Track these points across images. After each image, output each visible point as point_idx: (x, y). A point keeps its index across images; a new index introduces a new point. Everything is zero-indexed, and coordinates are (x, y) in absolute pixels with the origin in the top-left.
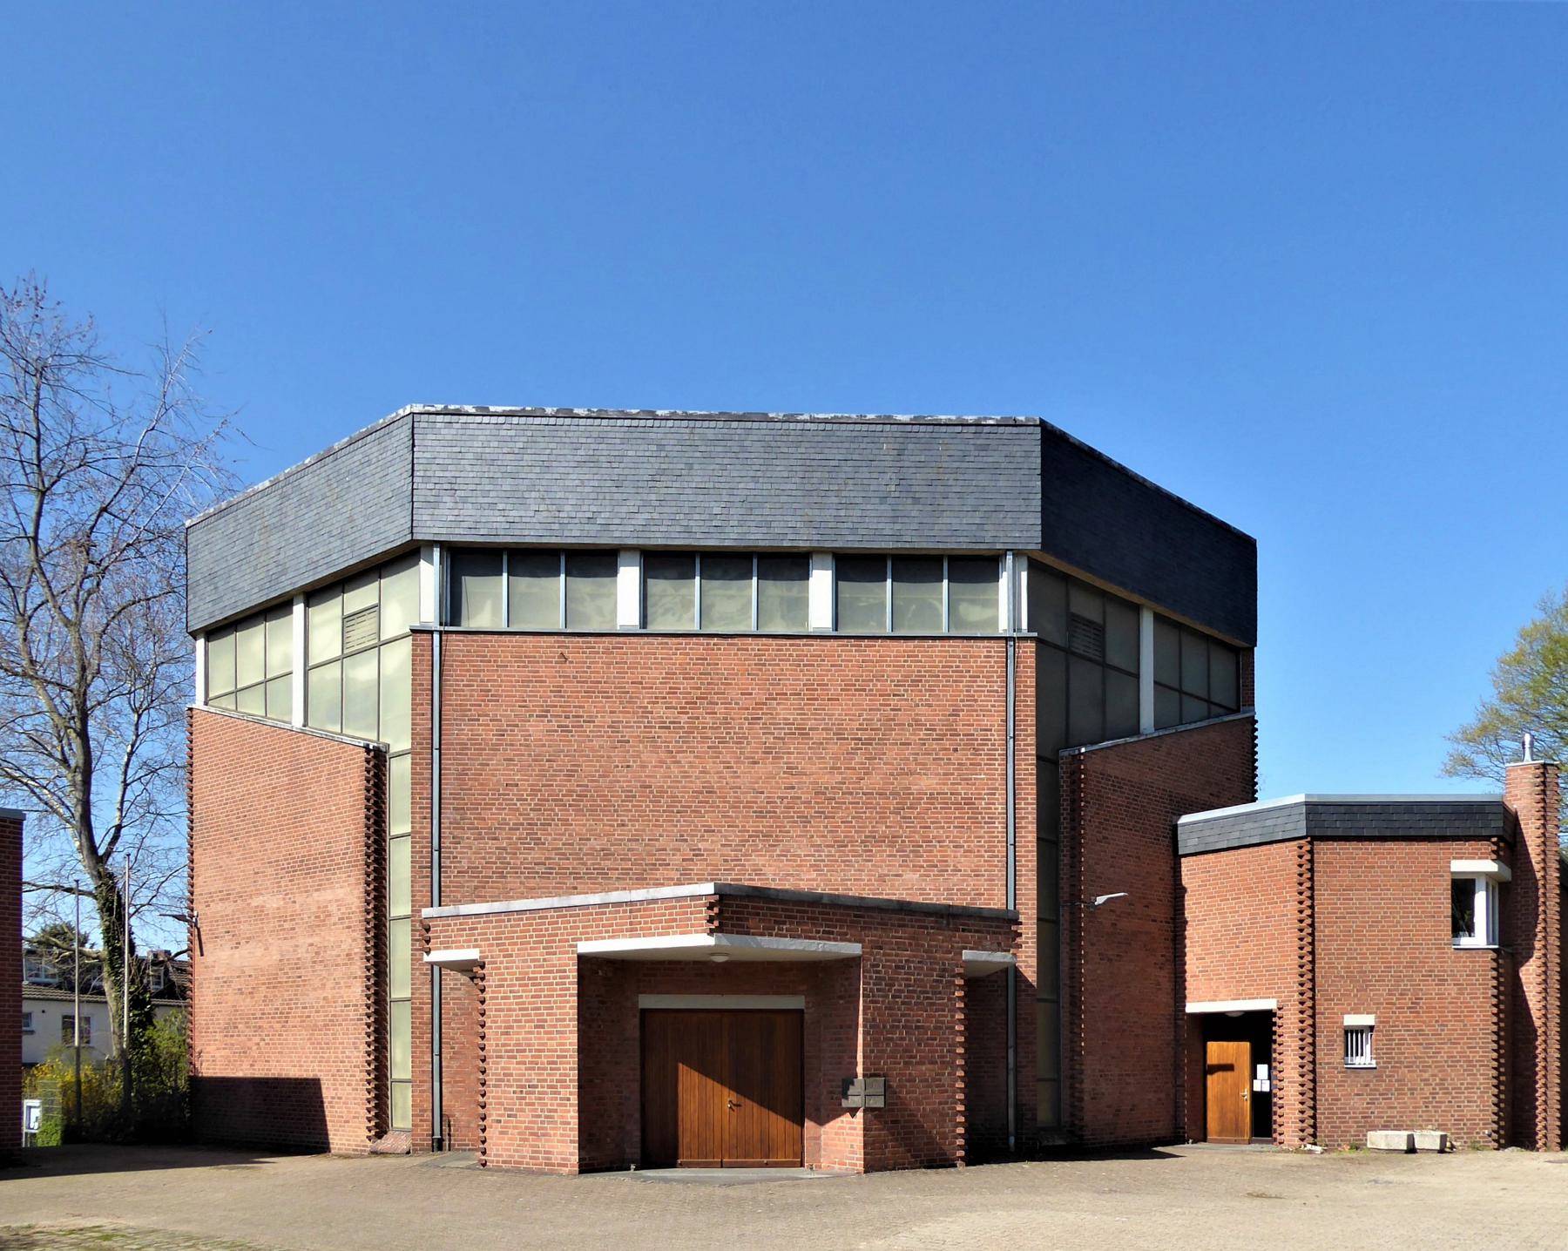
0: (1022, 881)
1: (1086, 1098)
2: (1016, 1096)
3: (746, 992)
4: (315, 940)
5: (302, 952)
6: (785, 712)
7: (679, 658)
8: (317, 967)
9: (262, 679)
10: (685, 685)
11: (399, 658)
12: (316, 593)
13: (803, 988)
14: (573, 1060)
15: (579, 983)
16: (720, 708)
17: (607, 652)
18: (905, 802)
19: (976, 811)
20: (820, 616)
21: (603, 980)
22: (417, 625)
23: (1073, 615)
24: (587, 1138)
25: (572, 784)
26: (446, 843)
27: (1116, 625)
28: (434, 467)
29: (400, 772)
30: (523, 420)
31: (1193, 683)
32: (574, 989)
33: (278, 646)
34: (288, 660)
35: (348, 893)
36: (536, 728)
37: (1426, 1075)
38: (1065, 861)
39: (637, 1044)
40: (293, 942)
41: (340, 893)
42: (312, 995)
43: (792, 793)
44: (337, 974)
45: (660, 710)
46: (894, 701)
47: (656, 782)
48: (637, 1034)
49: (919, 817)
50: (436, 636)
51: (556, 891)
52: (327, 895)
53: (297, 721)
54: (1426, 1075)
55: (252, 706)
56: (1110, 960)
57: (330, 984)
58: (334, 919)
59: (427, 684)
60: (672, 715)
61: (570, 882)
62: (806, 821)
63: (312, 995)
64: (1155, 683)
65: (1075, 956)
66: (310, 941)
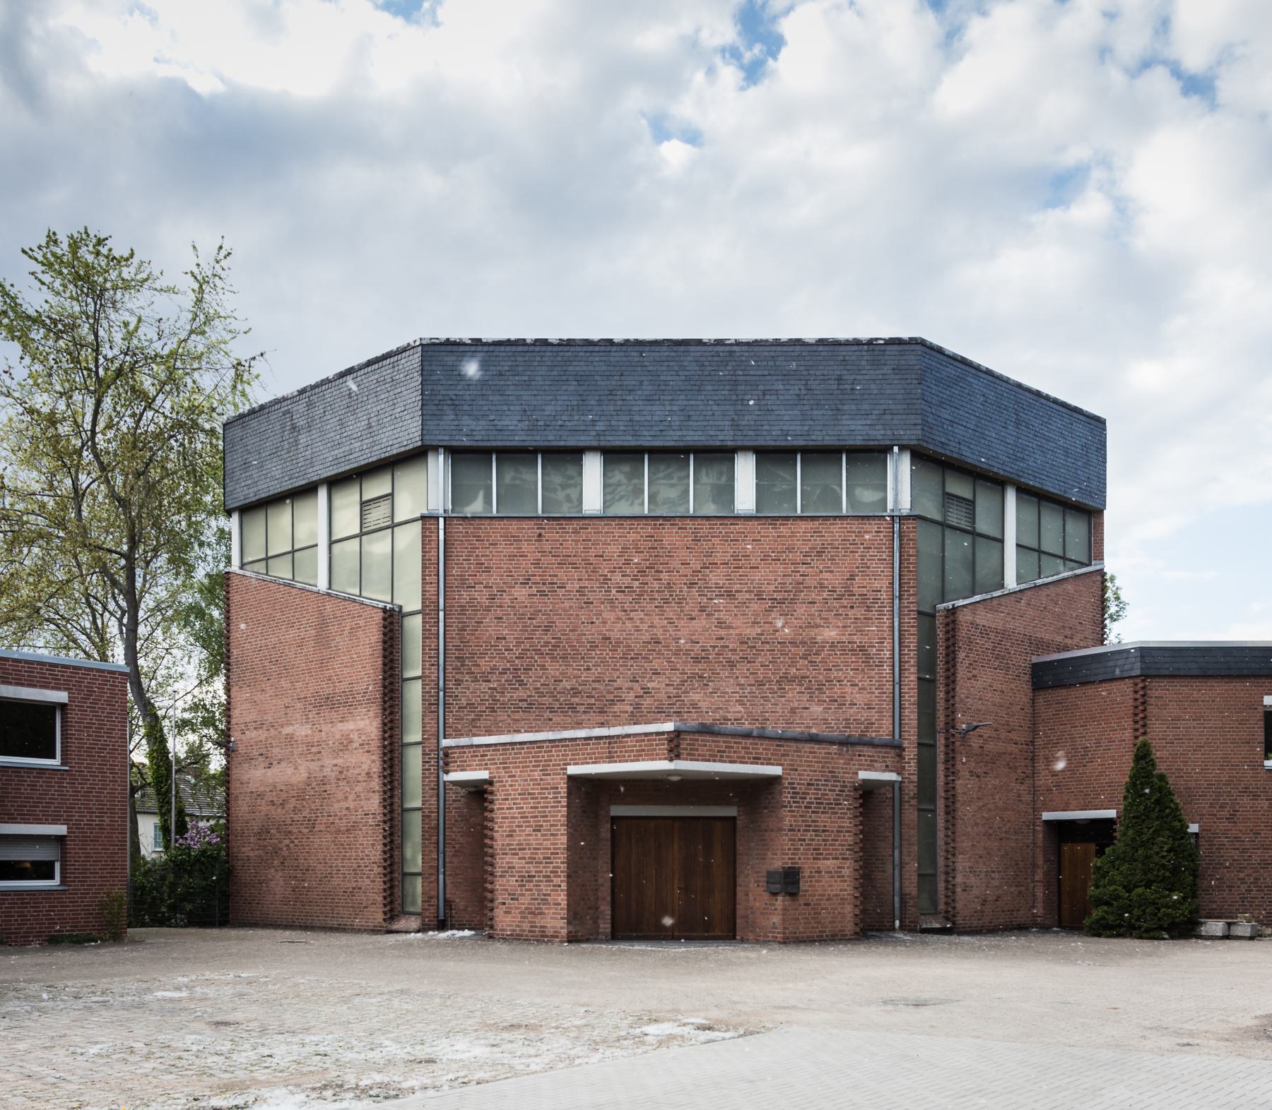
1: (959, 890)
2: (901, 887)
3: (643, 804)
4: (339, 761)
5: (327, 771)
6: (716, 577)
7: (632, 536)
9: (296, 554)
11: (410, 538)
12: (336, 482)
14: (563, 856)
15: (568, 797)
16: (664, 576)
17: (576, 532)
18: (811, 649)
20: (745, 497)
21: (589, 793)
22: (425, 512)
23: (948, 494)
24: (574, 915)
25: (547, 638)
27: (984, 503)
28: (439, 387)
29: (414, 626)
30: (508, 348)
31: (1051, 543)
32: (564, 802)
33: (310, 522)
34: (314, 534)
35: (366, 724)
36: (521, 593)
37: (1242, 875)
40: (320, 763)
41: (361, 724)
42: (336, 806)
43: (722, 643)
44: (358, 789)
45: (617, 578)
46: (802, 569)
47: (615, 635)
49: (823, 661)
50: (441, 520)
51: (549, 725)
52: (350, 726)
53: (322, 585)
54: (1242, 875)
55: (282, 571)
57: (351, 797)
58: (356, 745)
59: (434, 559)
60: (627, 581)
61: (547, 714)
62: (732, 664)
63: (336, 806)
64: (1018, 545)
65: (951, 771)
66: (335, 762)
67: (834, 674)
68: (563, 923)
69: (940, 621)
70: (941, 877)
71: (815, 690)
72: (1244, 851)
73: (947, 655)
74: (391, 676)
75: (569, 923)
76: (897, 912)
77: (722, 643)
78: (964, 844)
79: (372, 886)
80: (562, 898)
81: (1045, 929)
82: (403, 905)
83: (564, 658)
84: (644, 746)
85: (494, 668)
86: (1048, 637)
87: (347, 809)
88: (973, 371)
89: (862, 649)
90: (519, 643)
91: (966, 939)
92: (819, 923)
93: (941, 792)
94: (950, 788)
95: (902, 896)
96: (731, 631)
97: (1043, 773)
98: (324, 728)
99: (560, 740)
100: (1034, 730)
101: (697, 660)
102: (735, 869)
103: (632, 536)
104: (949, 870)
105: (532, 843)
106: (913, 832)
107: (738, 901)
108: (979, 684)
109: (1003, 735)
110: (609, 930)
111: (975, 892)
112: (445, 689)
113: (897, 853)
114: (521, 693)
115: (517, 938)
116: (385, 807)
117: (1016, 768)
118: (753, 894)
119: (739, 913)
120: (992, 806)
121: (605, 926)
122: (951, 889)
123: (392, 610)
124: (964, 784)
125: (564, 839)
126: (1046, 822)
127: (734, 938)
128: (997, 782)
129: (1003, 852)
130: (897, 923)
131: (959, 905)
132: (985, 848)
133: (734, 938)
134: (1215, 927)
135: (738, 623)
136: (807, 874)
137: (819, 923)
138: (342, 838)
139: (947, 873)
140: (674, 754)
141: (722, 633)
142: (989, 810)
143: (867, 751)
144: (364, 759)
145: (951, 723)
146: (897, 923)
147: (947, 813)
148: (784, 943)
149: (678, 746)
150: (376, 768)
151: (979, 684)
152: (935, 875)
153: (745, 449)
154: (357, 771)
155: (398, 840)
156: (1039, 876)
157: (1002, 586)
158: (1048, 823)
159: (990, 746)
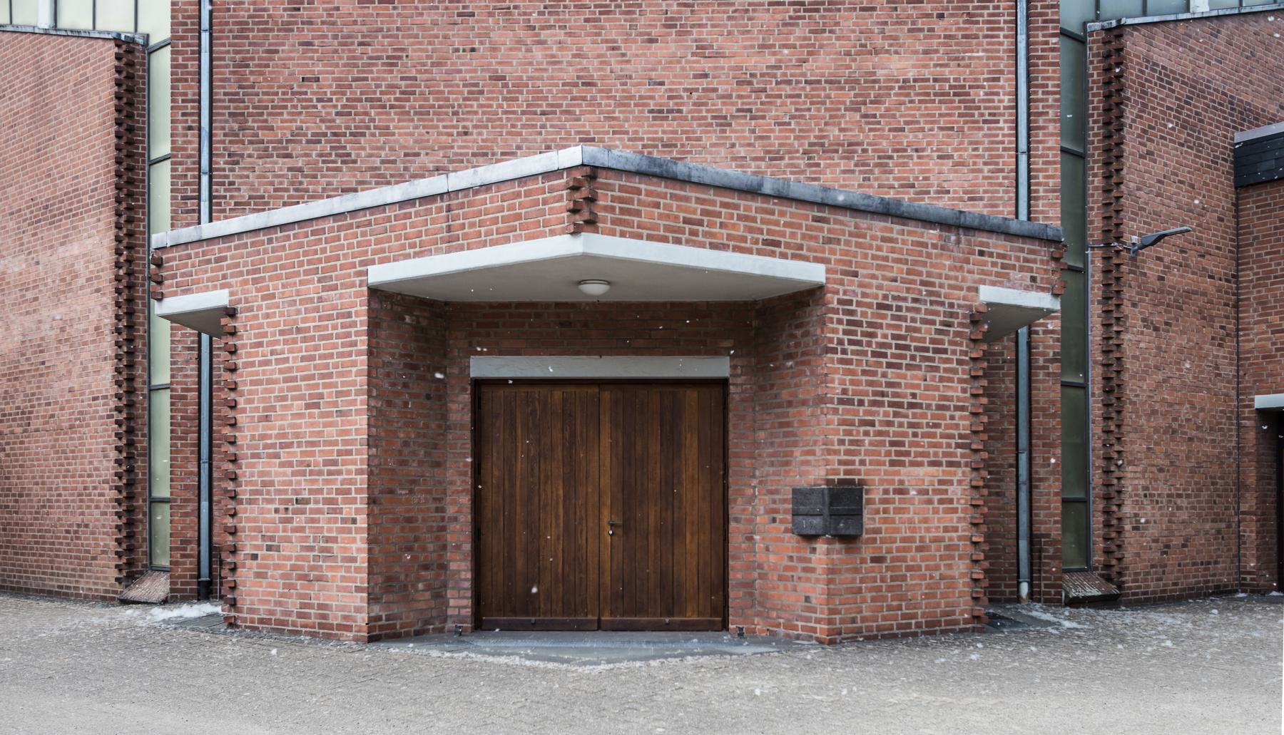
1: (1128, 527)
2: (1031, 522)
8: (64, 348)
13: (727, 344)
14: (360, 458)
15: (370, 333)
19: (971, 106)
21: (422, 330)
24: (385, 581)
25: (394, 77)
26: (221, 162)
29: (162, 64)
32: (362, 343)
38: (1096, 182)
39: (468, 434)
40: (36, 317)
43: (704, 83)
48: (467, 418)
52: (75, 249)
56: (1156, 329)
57: (76, 370)
58: (82, 281)
62: (723, 122)
65: (1112, 319)
67: (908, 137)
68: (360, 599)
69: (1094, 48)
70: (1097, 506)
73: (1107, 110)
74: (130, 156)
75: (372, 599)
76: (1024, 570)
78: (1134, 445)
79: (102, 522)
80: (358, 546)
81: (1258, 592)
82: (150, 555)
83: (423, 113)
84: (513, 207)
85: (299, 132)
86: (1258, 103)
87: (71, 390)
89: (960, 91)
90: (342, 88)
91: (1165, 619)
92: (901, 598)
93: (1095, 355)
94: (1112, 347)
95: (1032, 539)
96: (722, 62)
97: (1257, 328)
98: (43, 258)
99: (354, 213)
100: (1239, 259)
101: (660, 114)
102: (726, 487)
104: (1112, 490)
105: (308, 432)
106: (1053, 423)
107: (732, 551)
108: (1158, 168)
109: (1194, 260)
110: (467, 612)
111: (1153, 531)
112: (211, 170)
113: (1023, 458)
115: (279, 629)
116: (119, 384)
117: (1212, 319)
118: (765, 539)
119: (735, 576)
120: (1176, 383)
121: (460, 604)
122: (1113, 525)
123: (130, 42)
124: (1135, 340)
125: (361, 421)
126: (1260, 411)
127: (724, 626)
129: (1193, 463)
130: (1025, 588)
131: (1129, 555)
132: (1167, 455)
133: (724, 626)
135: (731, 47)
136: (877, 496)
137: (901, 598)
138: (65, 441)
139: (1107, 498)
140: (584, 216)
141: (706, 65)
142: (1173, 388)
143: (997, 245)
144: (92, 304)
145: (1113, 232)
146: (1025, 588)
147: (1108, 391)
148: (832, 643)
149: (591, 200)
150: (108, 320)
151: (1158, 168)
152: (1085, 502)
154: (82, 327)
155: (141, 443)
156: (1250, 502)
157: (1187, 9)
158: (1264, 414)
159: (1174, 277)
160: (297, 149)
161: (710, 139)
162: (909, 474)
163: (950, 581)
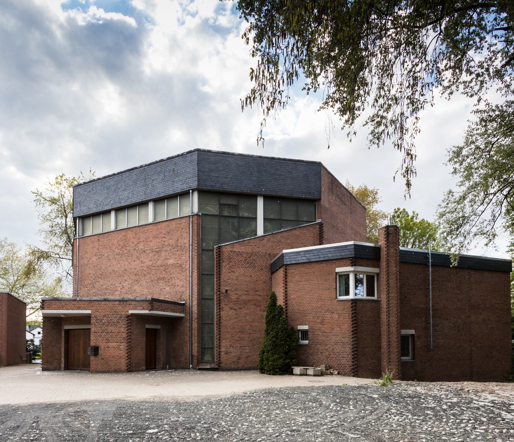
0: (194, 287)
6: (141, 246)
7: (120, 236)
10: (121, 243)
16: (128, 248)
36: (94, 259)
37: (326, 348)
43: (142, 268)
46: (164, 239)
54: (326, 348)
62: (145, 275)
65: (220, 309)
71: (167, 281)
72: (327, 337)
77: (142, 268)
88: (231, 156)
89: (181, 266)
103: (120, 236)
114: (94, 291)
128: (247, 311)
134: (297, 370)
135: (146, 261)
146: (191, 366)
153: (261, 195)
157: (256, 234)
160: (88, 286)
161: (143, 279)
162: (110, 344)
163: (121, 363)
